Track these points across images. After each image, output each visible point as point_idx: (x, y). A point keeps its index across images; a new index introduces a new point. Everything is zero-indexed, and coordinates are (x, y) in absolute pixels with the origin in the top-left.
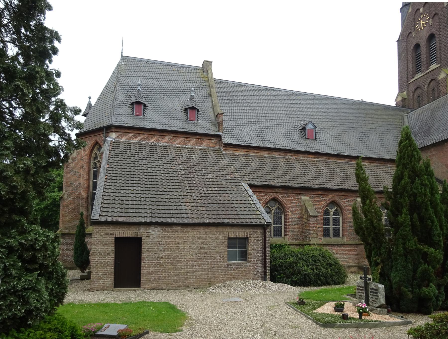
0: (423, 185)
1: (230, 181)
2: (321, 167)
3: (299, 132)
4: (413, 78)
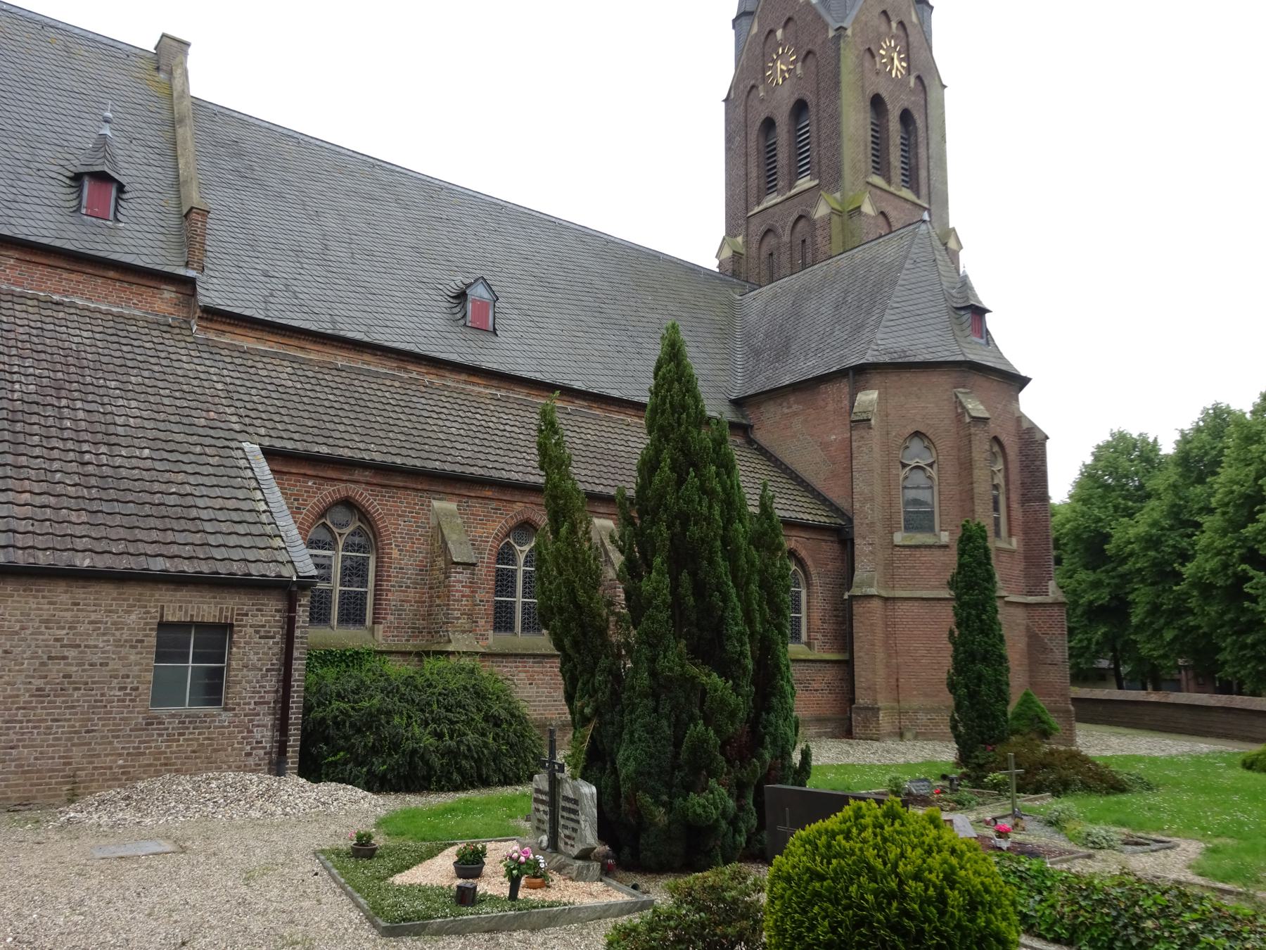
0: (705, 492)
1: (201, 431)
2: (502, 415)
3: (447, 305)
4: (759, 204)
